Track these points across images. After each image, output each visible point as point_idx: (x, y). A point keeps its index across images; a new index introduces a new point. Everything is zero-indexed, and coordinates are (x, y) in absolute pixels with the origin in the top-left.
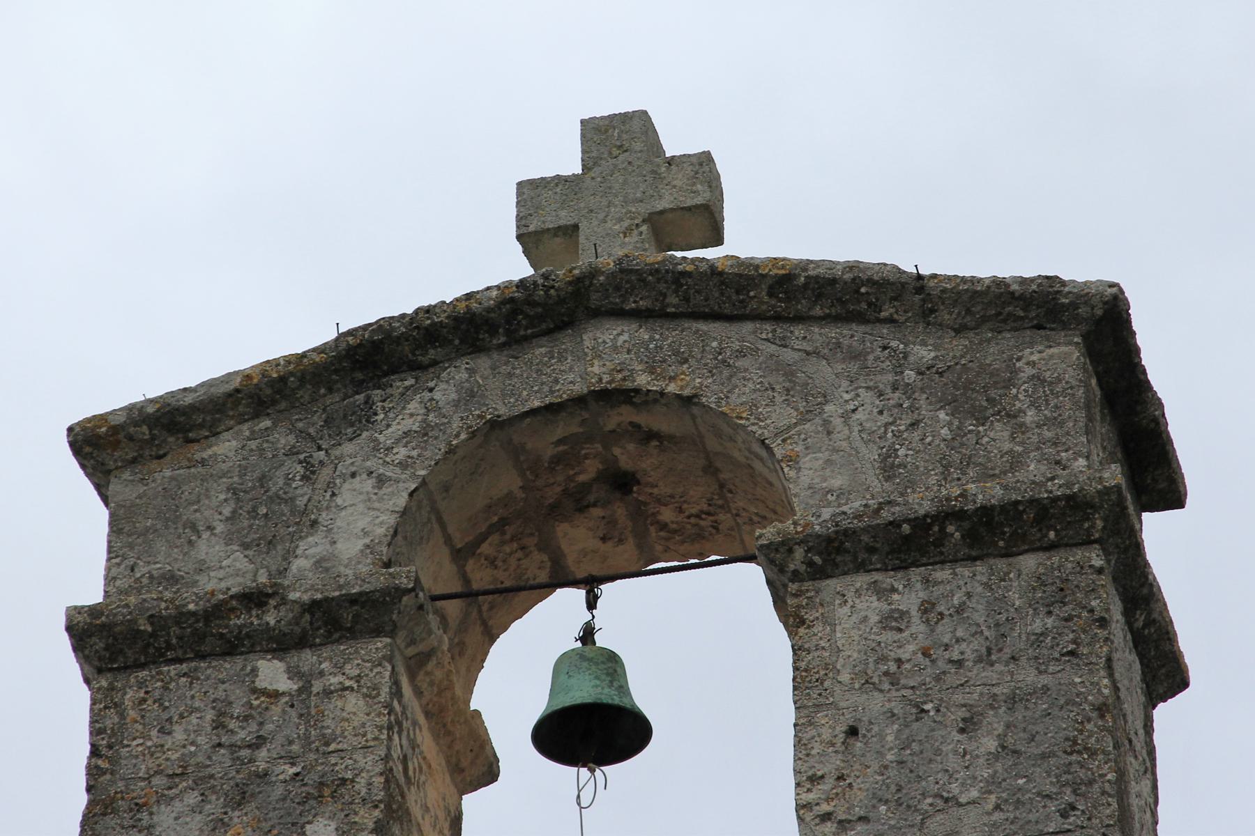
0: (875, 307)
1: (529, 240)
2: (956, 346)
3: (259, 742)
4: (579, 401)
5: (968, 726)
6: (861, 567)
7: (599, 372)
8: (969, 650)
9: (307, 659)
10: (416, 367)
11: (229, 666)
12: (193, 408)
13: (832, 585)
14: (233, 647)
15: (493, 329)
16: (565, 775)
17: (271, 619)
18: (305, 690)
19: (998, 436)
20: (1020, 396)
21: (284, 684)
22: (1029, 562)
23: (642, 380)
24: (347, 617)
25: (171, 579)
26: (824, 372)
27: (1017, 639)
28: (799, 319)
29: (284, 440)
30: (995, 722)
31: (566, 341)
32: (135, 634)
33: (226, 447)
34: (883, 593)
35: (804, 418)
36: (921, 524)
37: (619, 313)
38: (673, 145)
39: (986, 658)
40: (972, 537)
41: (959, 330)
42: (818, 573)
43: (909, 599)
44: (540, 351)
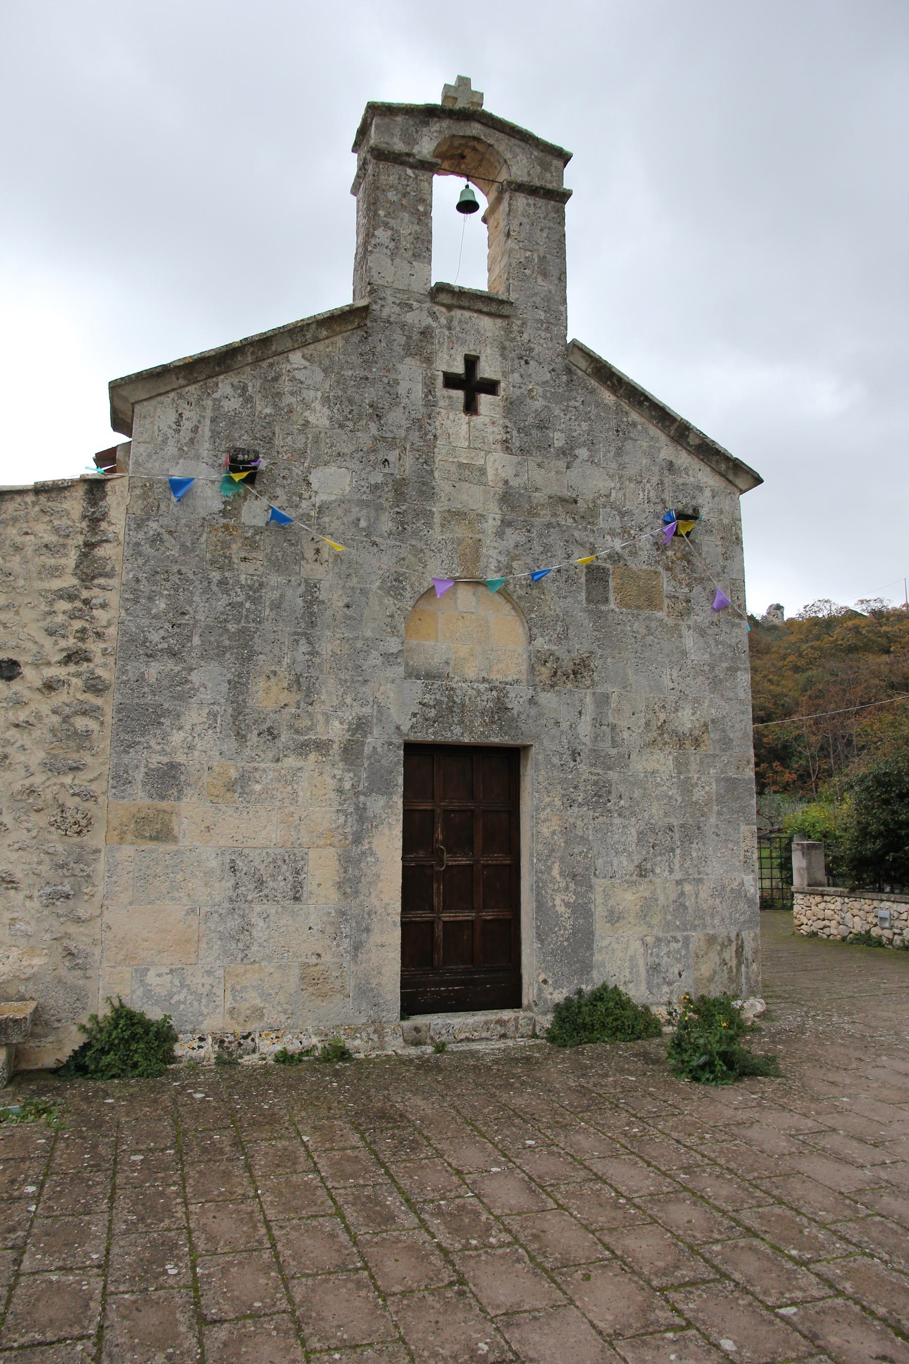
0: (528, 140)
1: (445, 97)
2: (542, 154)
3: (407, 186)
4: (469, 137)
5: (541, 230)
6: (523, 192)
7: (474, 132)
8: (542, 216)
9: (417, 172)
10: (439, 117)
11: (401, 167)
12: (395, 108)
13: (517, 194)
14: (403, 163)
15: (455, 114)
16: (463, 215)
17: (411, 160)
18: (416, 177)
19: (548, 175)
20: (553, 169)
21: (412, 175)
22: (552, 203)
23: (483, 137)
24: (426, 166)
25: (388, 143)
26: (518, 150)
27: (550, 216)
28: (513, 137)
29: (412, 123)
30: (546, 231)
31: (467, 123)
32: (383, 153)
33: (399, 119)
34: (527, 199)
35: (514, 157)
36: (537, 188)
37: (479, 121)
38: (473, 88)
39: (545, 218)
40: (544, 193)
41: (542, 151)
42: (515, 190)
43: (531, 202)
44: (462, 123)
